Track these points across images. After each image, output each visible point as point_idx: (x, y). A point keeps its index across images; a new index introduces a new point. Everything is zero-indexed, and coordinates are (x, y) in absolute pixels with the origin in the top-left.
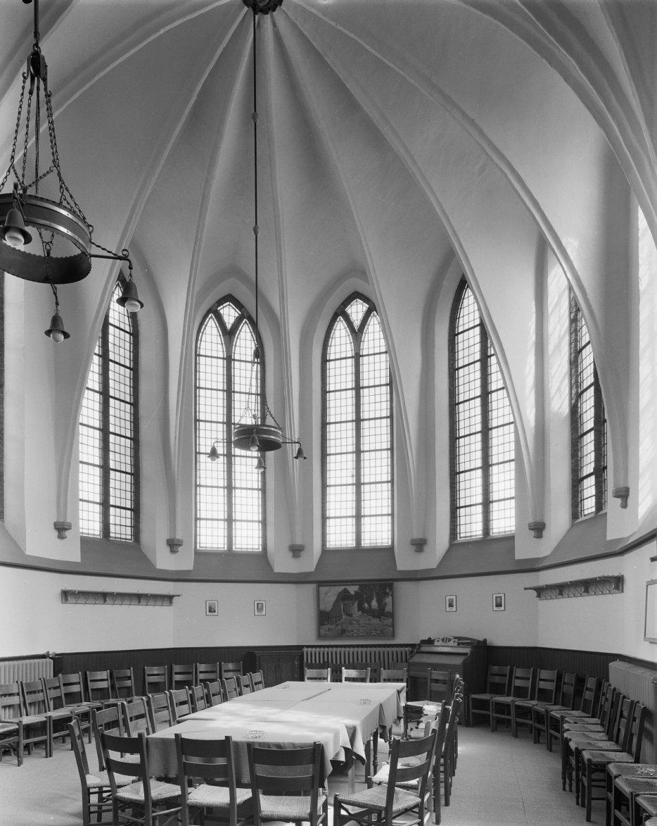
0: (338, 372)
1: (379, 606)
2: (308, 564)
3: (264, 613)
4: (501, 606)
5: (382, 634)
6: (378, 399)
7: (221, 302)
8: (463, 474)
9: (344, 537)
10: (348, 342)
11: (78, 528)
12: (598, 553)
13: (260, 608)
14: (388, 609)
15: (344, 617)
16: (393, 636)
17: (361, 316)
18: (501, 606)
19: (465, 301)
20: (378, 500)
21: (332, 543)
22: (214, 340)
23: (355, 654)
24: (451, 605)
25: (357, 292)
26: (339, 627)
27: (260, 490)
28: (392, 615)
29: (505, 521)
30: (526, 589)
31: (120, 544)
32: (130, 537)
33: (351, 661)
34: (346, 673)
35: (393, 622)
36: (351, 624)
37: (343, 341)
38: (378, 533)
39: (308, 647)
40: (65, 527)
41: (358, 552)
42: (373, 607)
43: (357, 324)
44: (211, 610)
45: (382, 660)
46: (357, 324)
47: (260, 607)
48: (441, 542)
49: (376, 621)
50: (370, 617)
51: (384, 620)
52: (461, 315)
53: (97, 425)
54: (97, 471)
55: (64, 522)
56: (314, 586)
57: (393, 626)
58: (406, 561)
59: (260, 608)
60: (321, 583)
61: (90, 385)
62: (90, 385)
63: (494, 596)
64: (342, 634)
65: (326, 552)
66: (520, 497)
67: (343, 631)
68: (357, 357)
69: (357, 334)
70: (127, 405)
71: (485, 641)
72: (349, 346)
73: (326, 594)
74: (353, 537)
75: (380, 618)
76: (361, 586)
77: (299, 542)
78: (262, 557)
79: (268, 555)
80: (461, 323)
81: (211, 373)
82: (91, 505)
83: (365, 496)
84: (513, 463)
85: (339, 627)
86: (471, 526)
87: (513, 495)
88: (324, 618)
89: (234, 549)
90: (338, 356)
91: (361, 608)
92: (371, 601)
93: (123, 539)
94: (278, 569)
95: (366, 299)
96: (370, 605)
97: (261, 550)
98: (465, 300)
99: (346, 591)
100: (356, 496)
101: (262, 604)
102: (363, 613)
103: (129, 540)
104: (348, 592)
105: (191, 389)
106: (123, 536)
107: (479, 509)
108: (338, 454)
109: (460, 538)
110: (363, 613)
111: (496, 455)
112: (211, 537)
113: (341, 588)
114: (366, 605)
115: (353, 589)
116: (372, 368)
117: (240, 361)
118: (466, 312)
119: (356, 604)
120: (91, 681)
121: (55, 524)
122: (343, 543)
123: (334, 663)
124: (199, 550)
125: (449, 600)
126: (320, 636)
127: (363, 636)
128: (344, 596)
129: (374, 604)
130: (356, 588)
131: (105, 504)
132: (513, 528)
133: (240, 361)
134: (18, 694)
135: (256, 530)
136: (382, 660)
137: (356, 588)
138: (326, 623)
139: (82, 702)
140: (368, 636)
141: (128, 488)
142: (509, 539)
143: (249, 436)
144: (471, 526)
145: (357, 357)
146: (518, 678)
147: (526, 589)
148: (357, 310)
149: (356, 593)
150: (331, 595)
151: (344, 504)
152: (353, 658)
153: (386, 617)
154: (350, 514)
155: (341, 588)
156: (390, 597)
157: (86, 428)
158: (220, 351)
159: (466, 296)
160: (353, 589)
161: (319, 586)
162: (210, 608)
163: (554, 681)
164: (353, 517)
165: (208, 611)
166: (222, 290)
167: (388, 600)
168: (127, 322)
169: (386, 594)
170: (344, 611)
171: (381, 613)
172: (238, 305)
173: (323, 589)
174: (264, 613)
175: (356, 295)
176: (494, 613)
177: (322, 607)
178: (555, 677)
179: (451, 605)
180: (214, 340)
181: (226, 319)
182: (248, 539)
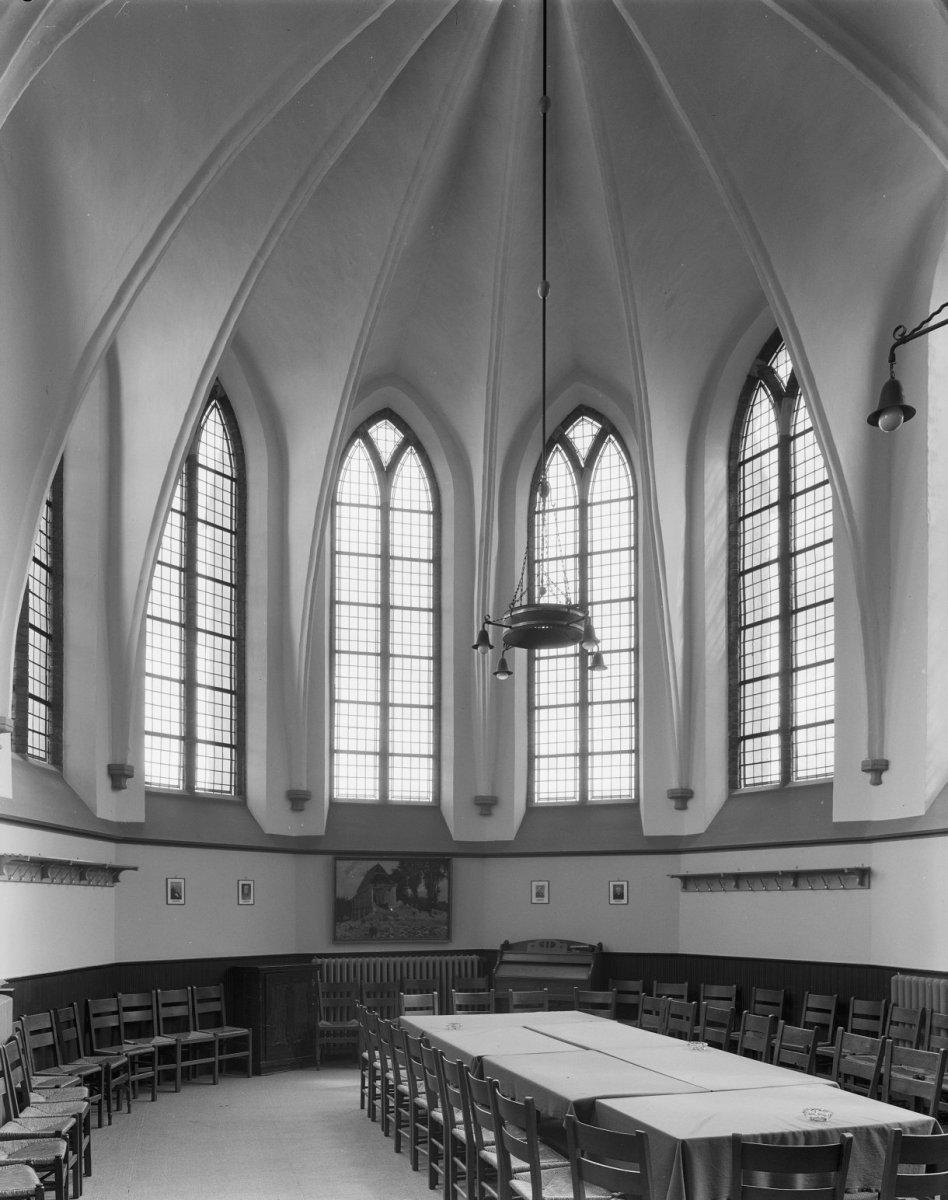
0: (615, 531)
1: (356, 897)
2: (313, 824)
3: (251, 902)
4: (622, 898)
5: (432, 935)
6: (415, 580)
7: (569, 420)
8: (751, 685)
9: (361, 785)
10: (422, 487)
11: (142, 775)
12: (19, 815)
13: (246, 891)
14: (442, 897)
15: (375, 909)
16: (448, 936)
17: (589, 442)
18: (622, 898)
19: (756, 410)
20: (414, 732)
21: (341, 792)
22: (415, 485)
23: (385, 967)
24: (540, 894)
25: (390, 410)
26: (367, 925)
27: (536, 708)
28: (447, 907)
29: (816, 757)
30: (135, 869)
31: (211, 801)
32: (227, 788)
33: (399, 977)
34: (458, 997)
35: (449, 917)
36: (386, 919)
37: (415, 485)
38: (413, 783)
39: (320, 956)
40: (126, 772)
41: (384, 810)
42: (420, 895)
43: (386, 458)
44: (175, 894)
45: (438, 974)
46: (386, 458)
47: (246, 891)
48: (712, 791)
49: (424, 915)
50: (414, 910)
51: (436, 913)
52: (750, 432)
53: (176, 619)
54: (176, 689)
55: (122, 765)
56: (330, 857)
57: (449, 923)
58: (462, 827)
59: (246, 891)
60: (340, 855)
61: (164, 556)
62: (164, 556)
63: (241, 883)
64: (372, 935)
65: (532, 810)
66: (842, 720)
67: (373, 931)
68: (583, 506)
69: (583, 471)
70: (225, 587)
71: (600, 945)
72: (570, 489)
73: (347, 872)
74: (375, 785)
75: (429, 911)
76: (402, 862)
77: (483, 790)
78: (627, 810)
79: (442, 808)
80: (748, 444)
81: (356, 529)
82: (166, 740)
83: (395, 724)
84: (831, 666)
85: (367, 925)
86: (763, 766)
87: (831, 716)
88: (342, 910)
89: (589, 798)
90: (606, 497)
91: (401, 895)
92: (417, 886)
93: (218, 791)
94: (649, 830)
95: (597, 415)
96: (415, 891)
97: (578, 800)
98: (755, 408)
99: (378, 868)
100: (381, 721)
101: (249, 885)
102: (405, 904)
103: (227, 792)
104: (383, 871)
105: (325, 555)
106: (218, 787)
107: (775, 741)
108: (616, 651)
109: (797, 778)
110: (405, 904)
111: (803, 655)
112: (555, 784)
113: (372, 864)
114: (410, 891)
115: (389, 867)
116: (606, 523)
117: (402, 510)
118: (757, 427)
119: (394, 889)
120: (778, 1005)
121: (110, 767)
122: (350, 792)
123: (418, 977)
124: (592, 801)
125: (537, 887)
126: (336, 940)
127: (403, 938)
128: (376, 877)
129: (422, 889)
130: (395, 865)
131: (189, 740)
132: (831, 770)
133: (402, 510)
134: (892, 1023)
135: (424, 770)
136: (438, 974)
137: (395, 865)
138: (346, 917)
139: (189, 1031)
140: (412, 937)
141: (227, 714)
142: (823, 789)
143: (558, 626)
144: (763, 766)
145: (583, 506)
146: (759, 1002)
147: (135, 869)
148: (583, 433)
149: (395, 872)
150: (354, 875)
151: (361, 733)
152: (401, 972)
153: (438, 910)
154: (425, 751)
155: (372, 864)
156: (445, 881)
157: (159, 623)
158: (372, 494)
159: (758, 400)
160: (389, 867)
161: (336, 859)
162: (173, 891)
163: (778, 1005)
164: (375, 753)
165: (612, 898)
166: (374, 402)
167: (443, 884)
168: (227, 462)
169: (440, 876)
170: (375, 900)
171: (431, 904)
172: (400, 423)
173: (343, 865)
174: (251, 902)
175: (581, 411)
176: (238, 908)
177: (340, 893)
178: (780, 999)
179: (540, 894)
180: (364, 479)
181: (380, 446)
182: (613, 780)
